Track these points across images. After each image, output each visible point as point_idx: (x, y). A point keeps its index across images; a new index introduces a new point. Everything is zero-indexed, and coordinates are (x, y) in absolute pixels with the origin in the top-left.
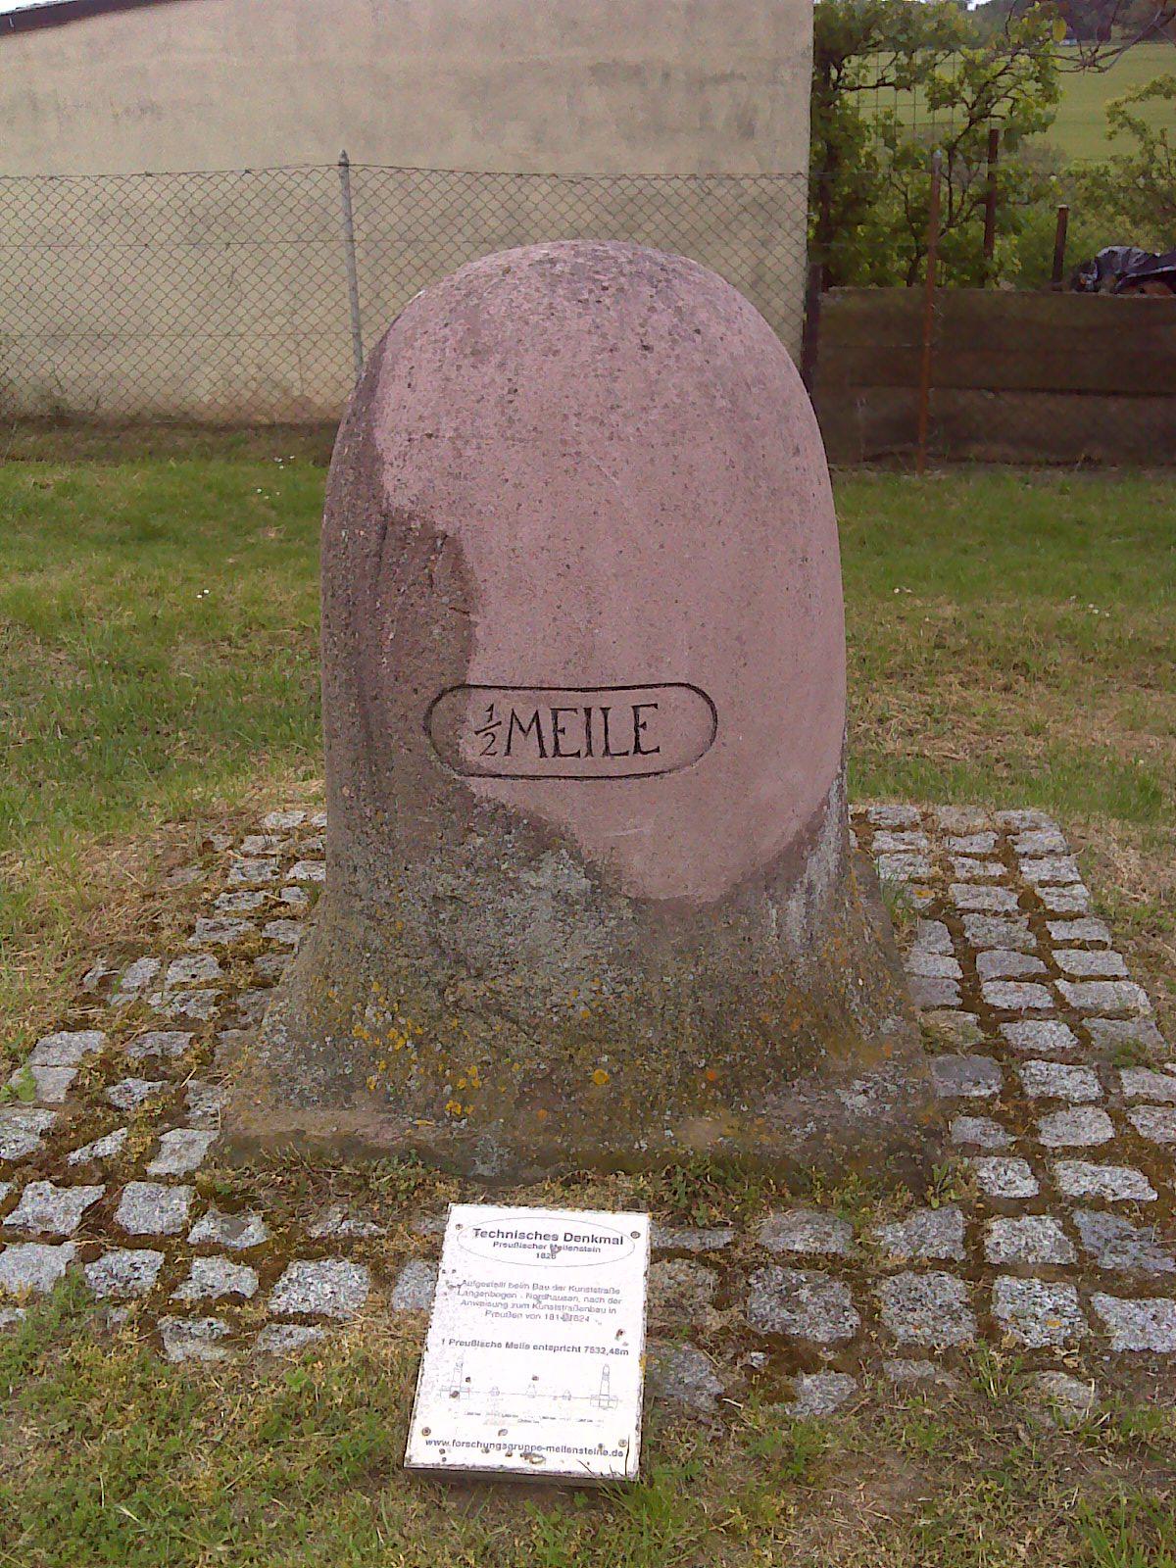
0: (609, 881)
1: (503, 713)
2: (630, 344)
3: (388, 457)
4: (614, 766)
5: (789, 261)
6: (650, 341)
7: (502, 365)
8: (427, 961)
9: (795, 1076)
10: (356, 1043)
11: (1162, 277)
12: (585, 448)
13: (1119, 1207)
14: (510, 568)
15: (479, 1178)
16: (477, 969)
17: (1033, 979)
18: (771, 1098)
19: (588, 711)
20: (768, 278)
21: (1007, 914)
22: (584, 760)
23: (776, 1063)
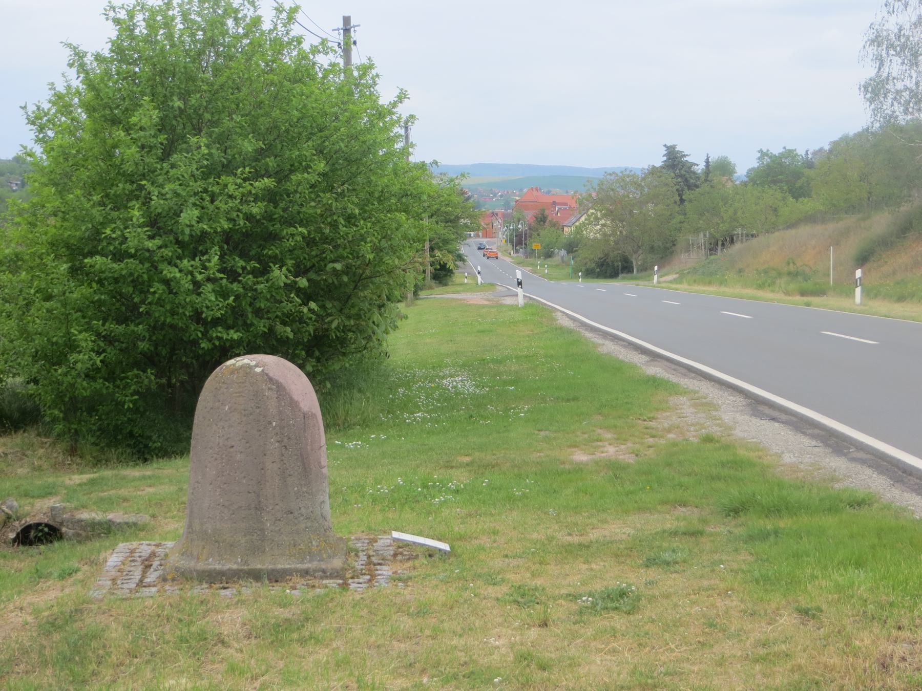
3: (300, 400)
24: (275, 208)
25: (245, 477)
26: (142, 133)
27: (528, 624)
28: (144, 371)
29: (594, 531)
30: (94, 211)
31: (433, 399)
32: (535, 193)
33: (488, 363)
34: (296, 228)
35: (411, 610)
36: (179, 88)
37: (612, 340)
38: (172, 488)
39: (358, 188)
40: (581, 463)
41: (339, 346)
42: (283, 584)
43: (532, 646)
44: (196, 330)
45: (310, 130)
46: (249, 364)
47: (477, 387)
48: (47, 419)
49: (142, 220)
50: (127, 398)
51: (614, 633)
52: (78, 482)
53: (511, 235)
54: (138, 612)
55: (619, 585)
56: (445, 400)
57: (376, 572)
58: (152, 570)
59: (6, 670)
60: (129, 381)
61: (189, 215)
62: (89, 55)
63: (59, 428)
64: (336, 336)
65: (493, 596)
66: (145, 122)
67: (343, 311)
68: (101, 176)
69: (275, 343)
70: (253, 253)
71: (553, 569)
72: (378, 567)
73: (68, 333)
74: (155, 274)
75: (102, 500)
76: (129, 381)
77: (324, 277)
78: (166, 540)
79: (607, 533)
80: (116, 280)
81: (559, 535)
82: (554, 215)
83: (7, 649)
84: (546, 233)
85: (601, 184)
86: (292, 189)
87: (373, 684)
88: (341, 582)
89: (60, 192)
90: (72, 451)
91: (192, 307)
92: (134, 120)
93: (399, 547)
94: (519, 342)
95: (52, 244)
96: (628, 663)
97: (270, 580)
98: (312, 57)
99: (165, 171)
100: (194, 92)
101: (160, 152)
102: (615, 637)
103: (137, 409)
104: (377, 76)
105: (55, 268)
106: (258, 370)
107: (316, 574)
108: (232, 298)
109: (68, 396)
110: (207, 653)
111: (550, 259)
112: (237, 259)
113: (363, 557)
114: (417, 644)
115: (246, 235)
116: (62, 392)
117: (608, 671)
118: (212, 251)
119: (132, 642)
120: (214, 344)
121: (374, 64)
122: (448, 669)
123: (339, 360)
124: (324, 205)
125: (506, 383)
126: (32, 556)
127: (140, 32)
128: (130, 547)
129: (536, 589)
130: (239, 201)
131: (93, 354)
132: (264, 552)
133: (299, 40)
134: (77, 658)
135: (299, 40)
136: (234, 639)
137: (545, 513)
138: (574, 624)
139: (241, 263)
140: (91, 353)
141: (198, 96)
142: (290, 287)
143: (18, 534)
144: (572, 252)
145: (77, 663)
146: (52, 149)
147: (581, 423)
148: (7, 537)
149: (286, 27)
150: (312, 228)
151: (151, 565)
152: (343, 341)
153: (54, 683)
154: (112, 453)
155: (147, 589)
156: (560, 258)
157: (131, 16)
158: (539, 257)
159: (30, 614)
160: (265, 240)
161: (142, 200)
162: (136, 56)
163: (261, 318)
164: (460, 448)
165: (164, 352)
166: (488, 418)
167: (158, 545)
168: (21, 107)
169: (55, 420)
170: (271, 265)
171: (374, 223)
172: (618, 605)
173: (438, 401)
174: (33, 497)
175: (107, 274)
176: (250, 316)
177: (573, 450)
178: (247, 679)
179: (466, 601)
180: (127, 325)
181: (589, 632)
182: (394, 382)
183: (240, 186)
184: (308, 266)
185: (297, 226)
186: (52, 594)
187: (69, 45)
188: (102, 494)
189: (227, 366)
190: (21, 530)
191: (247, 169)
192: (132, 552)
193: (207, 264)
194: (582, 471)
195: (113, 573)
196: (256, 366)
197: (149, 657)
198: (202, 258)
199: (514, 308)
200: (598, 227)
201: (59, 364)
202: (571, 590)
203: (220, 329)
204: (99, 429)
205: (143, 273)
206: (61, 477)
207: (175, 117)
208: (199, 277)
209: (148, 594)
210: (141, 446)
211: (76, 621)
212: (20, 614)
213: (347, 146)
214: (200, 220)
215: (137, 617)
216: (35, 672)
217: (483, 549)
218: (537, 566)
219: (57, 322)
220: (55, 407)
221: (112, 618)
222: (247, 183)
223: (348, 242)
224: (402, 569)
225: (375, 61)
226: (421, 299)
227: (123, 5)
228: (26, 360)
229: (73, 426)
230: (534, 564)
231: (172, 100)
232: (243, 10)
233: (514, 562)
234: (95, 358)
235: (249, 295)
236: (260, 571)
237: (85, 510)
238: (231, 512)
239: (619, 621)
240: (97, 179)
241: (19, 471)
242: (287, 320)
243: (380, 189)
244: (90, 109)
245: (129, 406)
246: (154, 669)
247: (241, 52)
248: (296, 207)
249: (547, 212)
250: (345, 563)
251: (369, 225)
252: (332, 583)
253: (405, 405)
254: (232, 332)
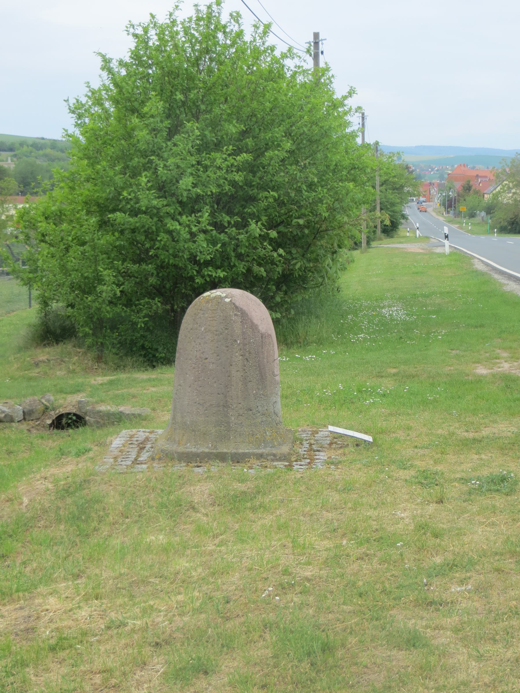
3: (259, 324)
24: (254, 177)
25: (215, 382)
26: (152, 120)
27: (428, 501)
28: (153, 299)
29: (487, 429)
30: (117, 178)
31: (374, 324)
32: (463, 168)
33: (418, 297)
34: (269, 192)
35: (339, 487)
36: (182, 85)
37: (515, 281)
38: (169, 388)
39: (317, 162)
40: (482, 375)
41: (301, 283)
42: (243, 465)
43: (430, 518)
44: (192, 269)
45: (281, 118)
46: (220, 296)
47: (407, 315)
48: (81, 335)
49: (149, 185)
50: (140, 320)
51: (494, 510)
52: (100, 382)
53: (444, 200)
54: (131, 483)
55: (501, 472)
56: (382, 325)
57: (315, 457)
58: (145, 451)
59: (30, 525)
60: (141, 307)
61: (186, 182)
62: (114, 61)
63: (89, 341)
64: (299, 275)
65: (402, 478)
66: (154, 111)
67: (305, 256)
68: (123, 151)
69: (252, 279)
70: (236, 211)
71: (451, 458)
72: (317, 453)
73: (96, 270)
74: (161, 226)
75: (117, 396)
76: (141, 307)
77: (291, 230)
78: (157, 428)
79: (496, 431)
80: (133, 231)
81: (459, 432)
82: (477, 185)
83: (32, 509)
84: (471, 199)
85: (513, 161)
86: (266, 162)
87: (304, 544)
88: (287, 464)
89: (92, 165)
90: (99, 359)
91: (189, 252)
92: (146, 109)
93: (335, 438)
94: (444, 281)
95: (86, 203)
96: (503, 534)
97: (233, 461)
98: (282, 61)
99: (169, 148)
100: (194, 88)
101: (165, 134)
102: (495, 513)
103: (148, 328)
104: (333, 76)
105: (87, 220)
106: (228, 300)
107: (269, 458)
108: (219, 245)
109: (96, 317)
110: (180, 516)
111: (473, 219)
112: (224, 215)
113: (306, 445)
114: (341, 514)
115: (232, 197)
116: (92, 314)
117: (487, 540)
118: (205, 210)
119: (125, 506)
120: (206, 280)
121: (330, 67)
122: (363, 534)
123: (301, 293)
124: (290, 175)
125: (430, 313)
126: (62, 438)
127: (154, 44)
128: (130, 433)
129: (436, 473)
130: (225, 171)
131: (114, 286)
132: (229, 439)
133: (272, 49)
134: (83, 517)
135: (272, 49)
136: (202, 506)
137: (450, 414)
138: (464, 501)
139: (227, 218)
140: (113, 285)
141: (196, 91)
142: (263, 237)
143: (53, 421)
144: (490, 214)
145: (83, 521)
146: (87, 132)
147: (484, 345)
148: (45, 423)
149: (262, 39)
150: (282, 193)
151: (145, 447)
152: (304, 279)
153: (65, 536)
154: (129, 360)
155: (139, 466)
156: (481, 218)
157: (146, 31)
158: (465, 217)
159: (52, 483)
160: (246, 201)
161: (153, 170)
162: (150, 62)
163: (242, 260)
164: (390, 362)
165: (168, 286)
166: (414, 340)
167: (151, 433)
168: (65, 100)
169: (86, 335)
170: (250, 220)
171: (328, 190)
172: (499, 488)
173: (377, 325)
174: (66, 393)
175: (126, 226)
176: (233, 259)
177: (477, 365)
178: (209, 537)
179: (381, 481)
180: (140, 264)
181: (475, 508)
182: (346, 310)
183: (226, 160)
184: (279, 222)
185: (270, 191)
186: (69, 468)
187: (100, 54)
188: (117, 392)
189: (204, 297)
190: (56, 418)
191: (231, 147)
192: (132, 437)
193: (200, 219)
194: (481, 382)
195: (115, 453)
196: (226, 297)
197: (137, 518)
198: (197, 215)
199: (443, 255)
200: (511, 195)
201: (89, 293)
202: (464, 475)
203: (210, 268)
204: (119, 343)
205: (153, 225)
206: (88, 378)
207: (179, 107)
208: (194, 229)
209: (140, 470)
210: (150, 356)
211: (84, 489)
212: (44, 483)
213: (309, 130)
214: (195, 185)
215: (130, 487)
216: (52, 527)
217: (399, 441)
218: (439, 455)
219: (88, 262)
220: (87, 325)
221: (111, 488)
222: (231, 157)
223: (310, 203)
224: (335, 455)
225: (330, 65)
226: (372, 247)
227: (140, 23)
228: (66, 289)
229: (100, 340)
230: (437, 453)
231: (176, 95)
232: (230, 26)
233: (421, 452)
234: (116, 289)
235: (233, 243)
236: (226, 453)
237: (103, 403)
238: (205, 408)
239: (499, 501)
240: (120, 154)
241: (58, 373)
242: (262, 262)
243: (334, 163)
244: (116, 102)
245: (141, 326)
246: (140, 528)
247: (229, 58)
248: (270, 176)
249: (471, 183)
250: (291, 449)
251: (325, 190)
252: (280, 464)
253: (352, 328)
254: (219, 271)
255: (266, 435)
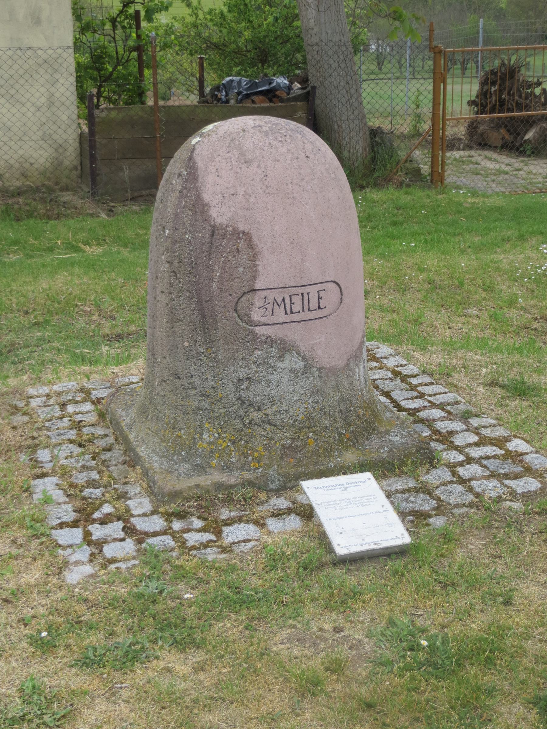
0: (310, 362)
1: (270, 299)
2: (302, 156)
3: (212, 204)
4: (312, 315)
5: (68, 94)
6: (308, 154)
7: (259, 166)
8: (235, 408)
9: (371, 433)
10: (200, 451)
11: (261, 93)
12: (295, 195)
13: (495, 457)
14: (272, 242)
15: (272, 490)
16: (258, 407)
17: (416, 398)
18: (367, 442)
19: (302, 295)
20: (57, 104)
21: (390, 379)
22: (302, 314)
23: (366, 429)
255: (201, 438)
